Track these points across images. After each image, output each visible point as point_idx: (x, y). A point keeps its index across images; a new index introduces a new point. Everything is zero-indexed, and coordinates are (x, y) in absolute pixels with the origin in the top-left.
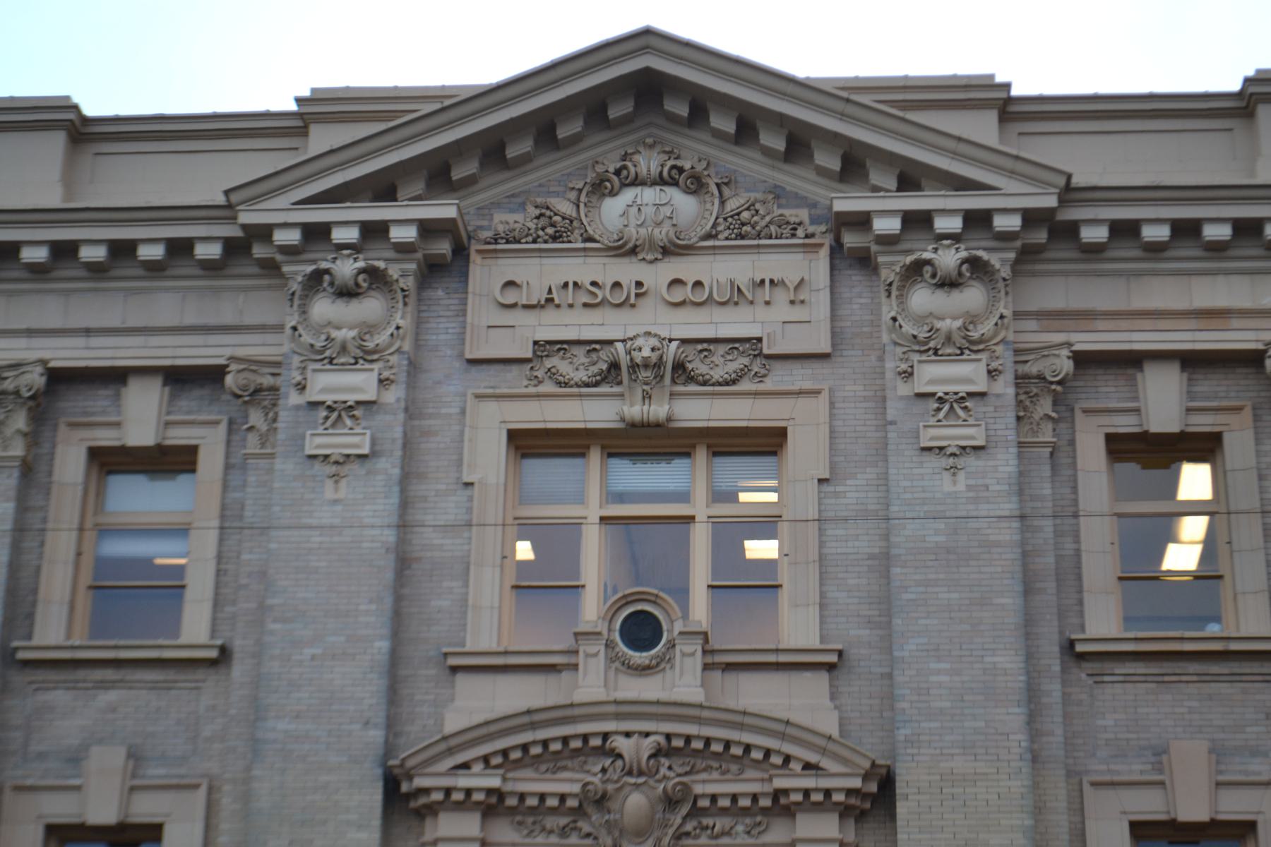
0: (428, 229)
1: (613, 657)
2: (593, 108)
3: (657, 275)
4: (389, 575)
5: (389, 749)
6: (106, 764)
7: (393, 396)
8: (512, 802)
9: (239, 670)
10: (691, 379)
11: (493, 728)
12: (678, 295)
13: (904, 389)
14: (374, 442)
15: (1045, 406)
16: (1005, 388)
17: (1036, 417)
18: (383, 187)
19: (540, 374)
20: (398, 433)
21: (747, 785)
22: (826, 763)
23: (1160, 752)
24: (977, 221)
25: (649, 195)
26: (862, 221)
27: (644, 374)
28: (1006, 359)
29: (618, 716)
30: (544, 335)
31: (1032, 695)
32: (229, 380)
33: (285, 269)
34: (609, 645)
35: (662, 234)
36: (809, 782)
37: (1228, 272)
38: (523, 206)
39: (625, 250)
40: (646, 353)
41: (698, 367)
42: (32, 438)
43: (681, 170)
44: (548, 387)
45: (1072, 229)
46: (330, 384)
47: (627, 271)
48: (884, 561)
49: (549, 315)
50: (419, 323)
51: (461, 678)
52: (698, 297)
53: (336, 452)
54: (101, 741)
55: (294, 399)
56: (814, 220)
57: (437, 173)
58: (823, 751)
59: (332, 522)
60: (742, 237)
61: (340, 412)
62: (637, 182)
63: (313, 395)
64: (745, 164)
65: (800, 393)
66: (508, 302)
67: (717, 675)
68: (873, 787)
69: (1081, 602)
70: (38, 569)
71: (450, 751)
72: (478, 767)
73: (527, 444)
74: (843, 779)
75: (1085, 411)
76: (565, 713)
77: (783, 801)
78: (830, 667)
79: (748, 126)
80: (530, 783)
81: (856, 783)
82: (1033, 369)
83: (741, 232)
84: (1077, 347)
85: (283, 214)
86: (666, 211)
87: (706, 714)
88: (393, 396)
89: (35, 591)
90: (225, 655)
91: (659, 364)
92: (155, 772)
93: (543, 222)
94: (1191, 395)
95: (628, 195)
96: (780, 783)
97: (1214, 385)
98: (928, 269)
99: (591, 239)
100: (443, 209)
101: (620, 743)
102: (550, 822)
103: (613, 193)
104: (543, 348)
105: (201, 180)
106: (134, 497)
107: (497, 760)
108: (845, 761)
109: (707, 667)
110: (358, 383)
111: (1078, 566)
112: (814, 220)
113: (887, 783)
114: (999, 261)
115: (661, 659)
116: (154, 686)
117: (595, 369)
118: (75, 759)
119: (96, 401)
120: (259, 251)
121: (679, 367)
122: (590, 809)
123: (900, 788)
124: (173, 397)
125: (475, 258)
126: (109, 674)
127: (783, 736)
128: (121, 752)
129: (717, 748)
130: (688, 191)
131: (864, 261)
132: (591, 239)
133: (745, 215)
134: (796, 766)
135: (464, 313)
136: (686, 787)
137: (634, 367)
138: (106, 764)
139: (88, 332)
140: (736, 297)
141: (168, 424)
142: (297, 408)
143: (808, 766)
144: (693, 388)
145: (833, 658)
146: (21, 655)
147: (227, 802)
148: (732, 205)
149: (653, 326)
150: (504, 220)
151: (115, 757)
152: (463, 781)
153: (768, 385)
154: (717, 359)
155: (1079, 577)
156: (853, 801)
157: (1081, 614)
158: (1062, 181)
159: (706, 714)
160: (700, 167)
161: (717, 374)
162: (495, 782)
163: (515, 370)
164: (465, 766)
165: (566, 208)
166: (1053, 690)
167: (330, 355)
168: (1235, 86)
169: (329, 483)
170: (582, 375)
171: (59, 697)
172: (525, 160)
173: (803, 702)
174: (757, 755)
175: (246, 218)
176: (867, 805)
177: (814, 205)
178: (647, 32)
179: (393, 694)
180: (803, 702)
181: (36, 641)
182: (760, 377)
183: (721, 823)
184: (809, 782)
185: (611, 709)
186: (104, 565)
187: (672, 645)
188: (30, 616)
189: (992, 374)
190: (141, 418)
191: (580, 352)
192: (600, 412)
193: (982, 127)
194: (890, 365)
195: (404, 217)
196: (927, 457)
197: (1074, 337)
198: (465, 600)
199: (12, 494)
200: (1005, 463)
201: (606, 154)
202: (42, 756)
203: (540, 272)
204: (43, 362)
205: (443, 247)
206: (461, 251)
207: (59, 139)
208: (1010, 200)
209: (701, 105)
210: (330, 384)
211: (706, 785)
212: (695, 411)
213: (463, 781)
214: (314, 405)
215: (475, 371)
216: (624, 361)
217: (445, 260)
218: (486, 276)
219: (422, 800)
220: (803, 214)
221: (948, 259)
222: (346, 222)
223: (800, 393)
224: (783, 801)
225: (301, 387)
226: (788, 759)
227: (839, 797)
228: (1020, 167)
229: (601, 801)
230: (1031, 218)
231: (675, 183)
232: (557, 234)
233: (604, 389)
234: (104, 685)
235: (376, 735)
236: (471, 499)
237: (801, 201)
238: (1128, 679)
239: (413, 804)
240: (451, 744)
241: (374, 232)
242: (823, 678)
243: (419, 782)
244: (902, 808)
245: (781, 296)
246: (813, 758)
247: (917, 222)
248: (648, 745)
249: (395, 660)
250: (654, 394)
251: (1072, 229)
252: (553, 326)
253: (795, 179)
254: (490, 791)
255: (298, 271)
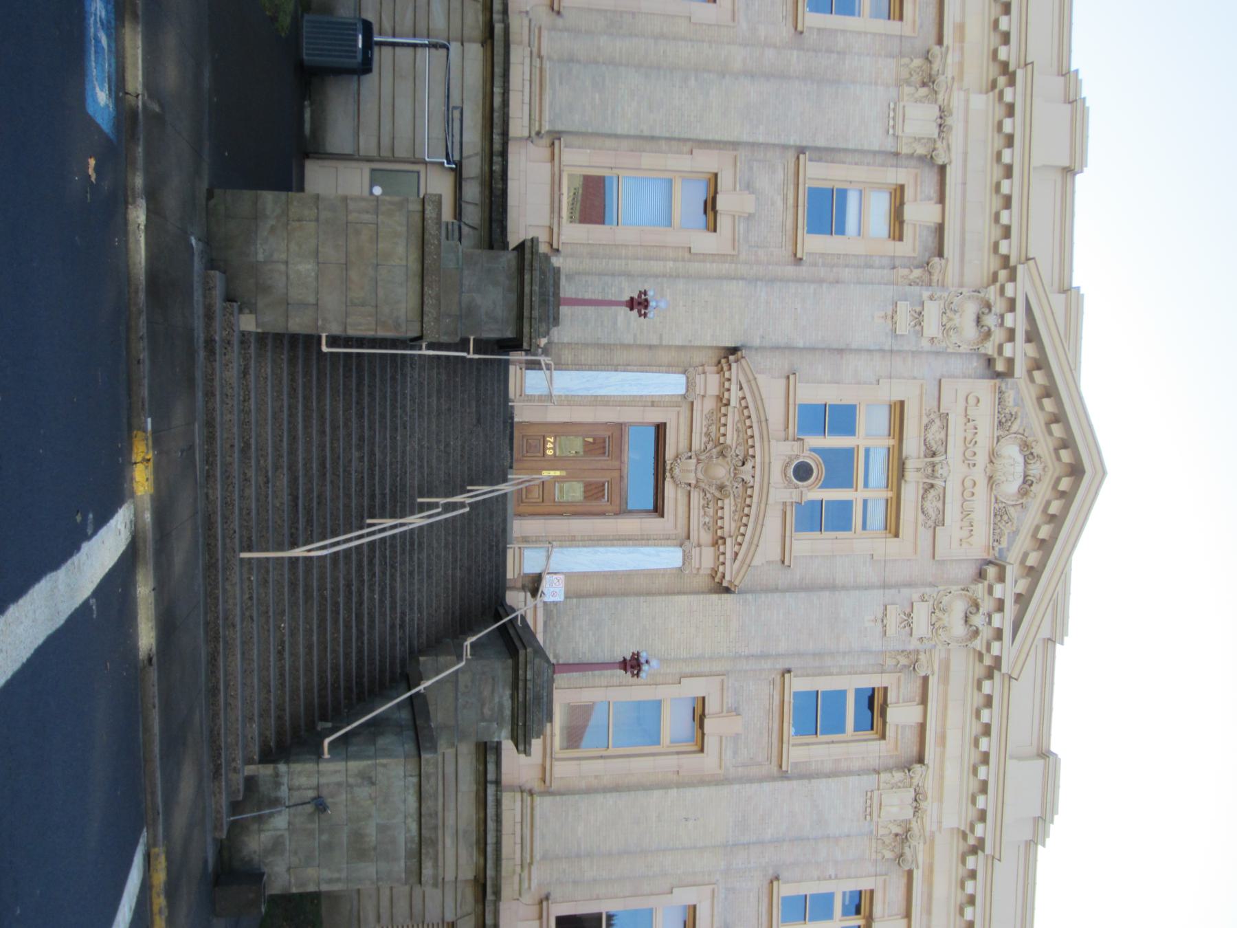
0: (1010, 362)
1: (791, 459)
2: (1067, 443)
3: (979, 475)
4: (835, 346)
5: (750, 348)
6: (747, 203)
7: (925, 344)
8: (723, 410)
9: (791, 270)
10: (926, 491)
11: (759, 402)
12: (968, 483)
13: (916, 597)
14: (902, 336)
15: (904, 661)
16: (914, 644)
17: (899, 657)
18: (1033, 336)
19: (932, 416)
20: (906, 348)
21: (729, 525)
22: (738, 562)
23: (736, 711)
24: (999, 634)
25: (1020, 469)
26: (1001, 578)
27: (929, 470)
28: (927, 645)
29: (763, 463)
30: (951, 418)
31: (764, 656)
32: (936, 259)
33: (992, 288)
34: (797, 456)
35: (998, 477)
36: (729, 555)
37: (962, 746)
38: (1016, 405)
39: (993, 457)
40: (940, 471)
41: (932, 493)
42: (911, 156)
43: (1031, 485)
44: (925, 420)
45: (990, 676)
46: (932, 312)
47: (982, 459)
48: (832, 587)
49: (962, 420)
50: (961, 354)
51: (784, 381)
52: (967, 494)
53: (898, 317)
54: (757, 199)
55: (926, 294)
56: (1001, 550)
57: (1040, 364)
58: (743, 562)
59: (861, 314)
60: (995, 515)
61: (919, 317)
62: (1026, 463)
63: (928, 304)
64: (1033, 515)
65: (916, 544)
66: (972, 399)
67: (780, 507)
68: (725, 584)
69: (808, 675)
70: (844, 163)
71: (749, 381)
72: (740, 394)
73: (898, 410)
74: (730, 572)
75: (899, 679)
76: (766, 438)
77: (720, 542)
78: (783, 562)
79: (1056, 520)
80: (732, 417)
81: (727, 577)
82: (922, 657)
83: (999, 514)
84: (931, 678)
85: (1019, 289)
86: (1011, 478)
87: (763, 506)
88: (925, 344)
89: (832, 162)
90: (798, 261)
91: (934, 477)
92: (742, 227)
93: (1008, 416)
94: (904, 727)
95: (1020, 459)
96: (728, 541)
97: (911, 737)
98: (974, 611)
99: (998, 441)
100: (1020, 369)
101: (749, 465)
102: (713, 428)
103: (1021, 451)
104: (945, 417)
105: (1040, 246)
106: (879, 206)
107: (743, 403)
108: (738, 572)
109: (785, 504)
110: (932, 327)
111: (825, 675)
112: (1001, 550)
113: (727, 590)
114: (979, 644)
115: (790, 482)
116: (783, 224)
117: (933, 443)
118: (749, 187)
119: (931, 189)
120: (1003, 274)
121: (932, 486)
122: (718, 448)
123: (725, 596)
124: (928, 227)
125: (992, 382)
126: (791, 201)
127: (751, 543)
128: (752, 211)
129: (746, 510)
130: (1020, 489)
131: (981, 575)
132: (998, 441)
133: (1005, 518)
134: (736, 548)
135: (964, 377)
136: (728, 496)
137: (934, 465)
138: (747, 203)
139: (964, 184)
140: (966, 514)
141: (915, 225)
142: (921, 296)
143: (736, 554)
144: (921, 492)
145: (787, 563)
146: (802, 156)
147: (725, 268)
148: (1011, 510)
149: (954, 469)
150: (1010, 396)
151: (750, 209)
152: (734, 388)
153: (921, 529)
154: (935, 503)
155: (820, 675)
156: (719, 575)
157: (802, 676)
158: (1014, 675)
159: (763, 506)
160: (1032, 494)
161: (927, 505)
162: (733, 403)
163: (936, 403)
164: (741, 388)
165: (1015, 428)
166: (766, 665)
167: (949, 309)
168: (1053, 749)
169: (883, 314)
170: (930, 436)
171: (780, 176)
172: (1042, 408)
173: (769, 548)
174: (742, 530)
175: (1020, 269)
176: (717, 580)
177: (1008, 549)
178: (1104, 473)
179: (776, 348)
180: (769, 548)
181: (808, 163)
182: (925, 525)
183: (711, 511)
184: (729, 555)
185: (767, 460)
186: (843, 193)
187: (796, 487)
188: (820, 160)
189: (921, 639)
190: (920, 213)
191: (943, 435)
192: (912, 446)
193: (1045, 632)
194: (928, 590)
195: (1020, 351)
196: (882, 608)
197: (936, 677)
198: (821, 382)
199: (883, 149)
200: (876, 645)
201: (1043, 447)
202: (751, 168)
203: (984, 416)
204: (950, 162)
205: (1000, 366)
206: (998, 375)
207: (1066, 163)
208: (1005, 650)
209: (1067, 497)
210: (932, 312)
211: (729, 504)
212: (910, 492)
213: (734, 388)
214: (923, 304)
215: (937, 383)
216: (936, 459)
217: (995, 370)
218: (984, 388)
219: (725, 368)
220: (1004, 545)
221: (978, 620)
222: (1016, 321)
223: (916, 544)
224: (720, 542)
225: (931, 298)
226: (740, 544)
227: (721, 568)
228: (1023, 656)
229: (722, 454)
230: (998, 659)
231: (1024, 482)
232: (1004, 422)
233: (923, 448)
234: (785, 200)
235: (757, 342)
236: (871, 383)
237: (1010, 544)
238: (771, 696)
239: (723, 361)
240: (752, 381)
241: (1011, 335)
242: (778, 558)
243: (734, 366)
244: (715, 597)
245: (965, 533)
246: (740, 557)
247: (1000, 606)
248: (748, 478)
249: (791, 349)
250: (919, 474)
251: (990, 676)
252: (956, 422)
253: (1023, 542)
254: (729, 400)
255: (992, 293)
